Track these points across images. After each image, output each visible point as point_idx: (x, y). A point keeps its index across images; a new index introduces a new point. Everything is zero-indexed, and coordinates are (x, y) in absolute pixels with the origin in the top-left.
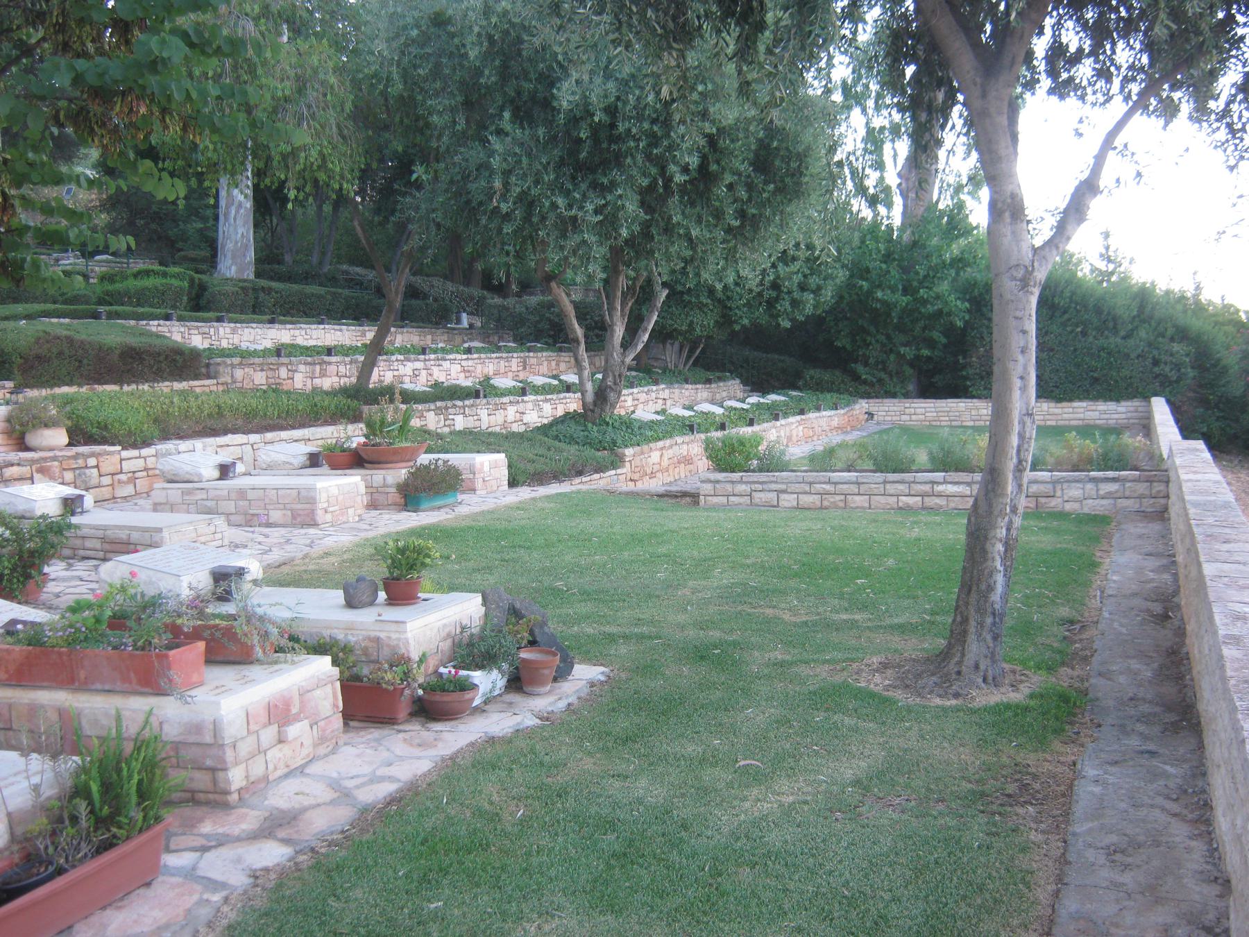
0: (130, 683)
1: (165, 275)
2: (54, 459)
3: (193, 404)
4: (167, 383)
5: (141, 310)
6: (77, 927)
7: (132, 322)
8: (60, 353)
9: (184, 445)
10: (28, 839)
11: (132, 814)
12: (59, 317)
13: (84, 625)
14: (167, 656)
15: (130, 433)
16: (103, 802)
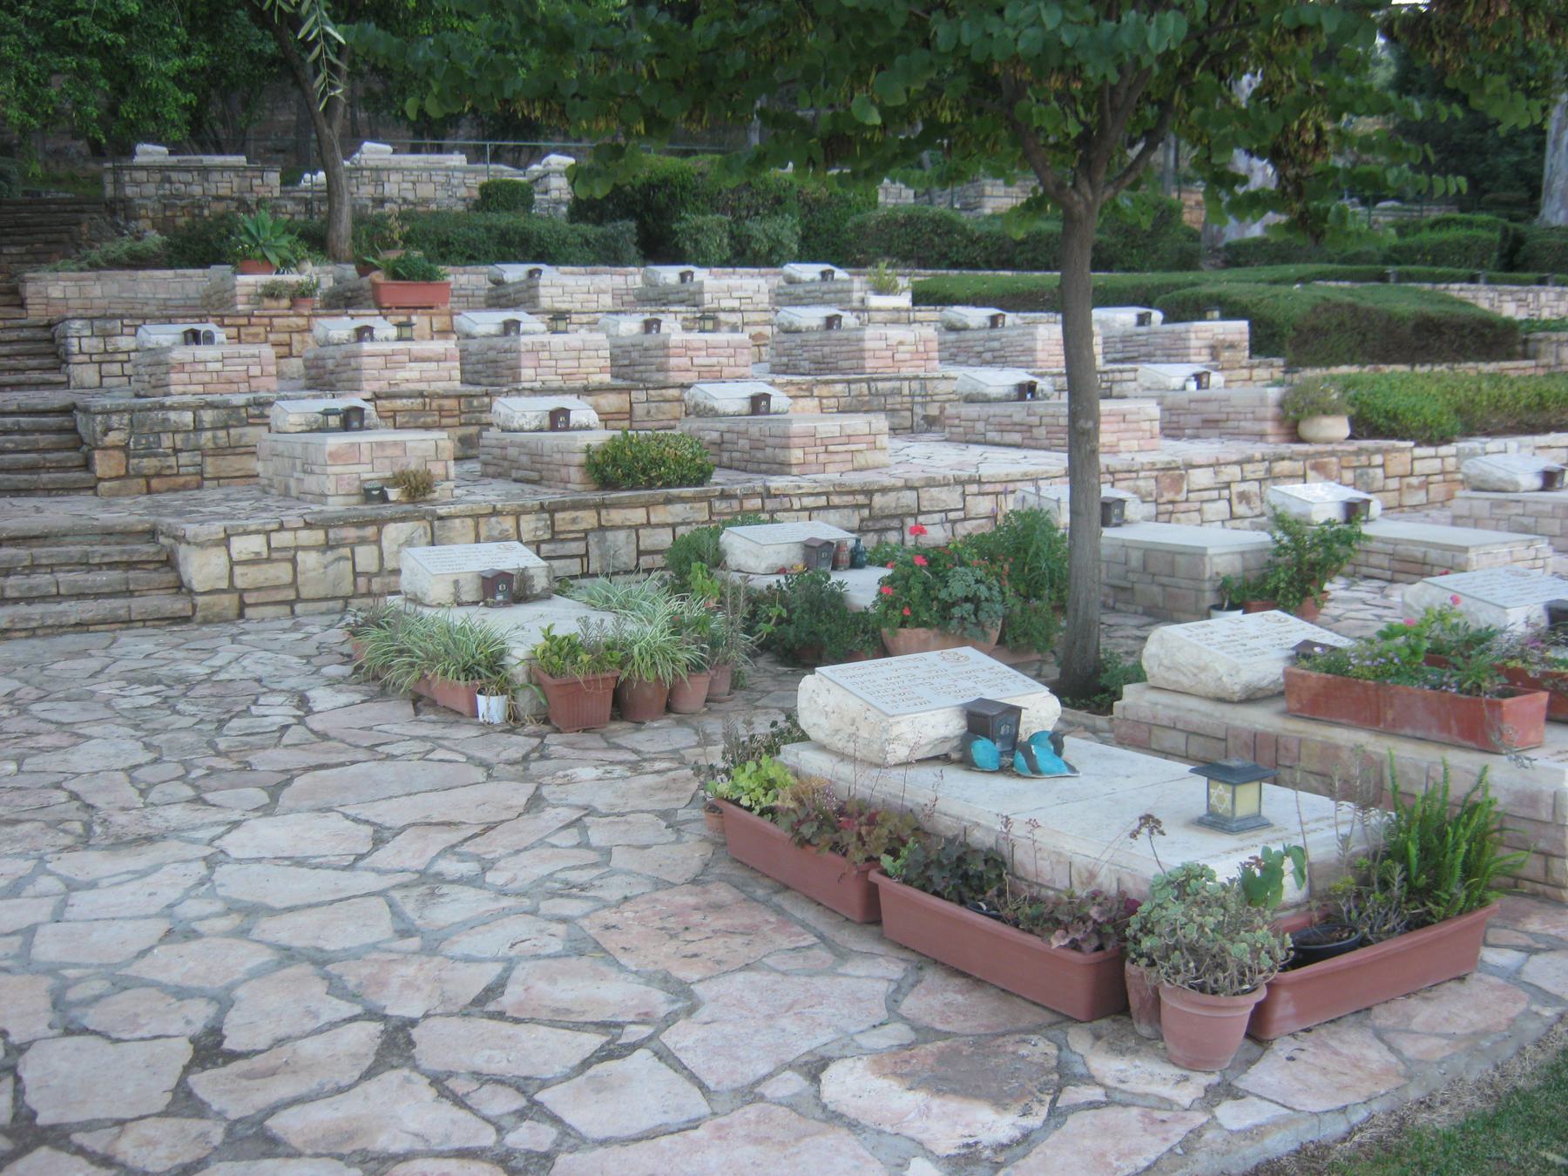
0: (1450, 731)
1: (1470, 224)
2: (1332, 454)
3: (1507, 391)
4: (1471, 364)
5: (1439, 270)
6: (1376, 1010)
7: (1427, 286)
8: (1341, 324)
9: (1494, 444)
10: (1328, 896)
11: (1454, 890)
12: (1337, 280)
13: (1398, 655)
14: (1500, 705)
15: (1425, 427)
16: (1421, 870)
